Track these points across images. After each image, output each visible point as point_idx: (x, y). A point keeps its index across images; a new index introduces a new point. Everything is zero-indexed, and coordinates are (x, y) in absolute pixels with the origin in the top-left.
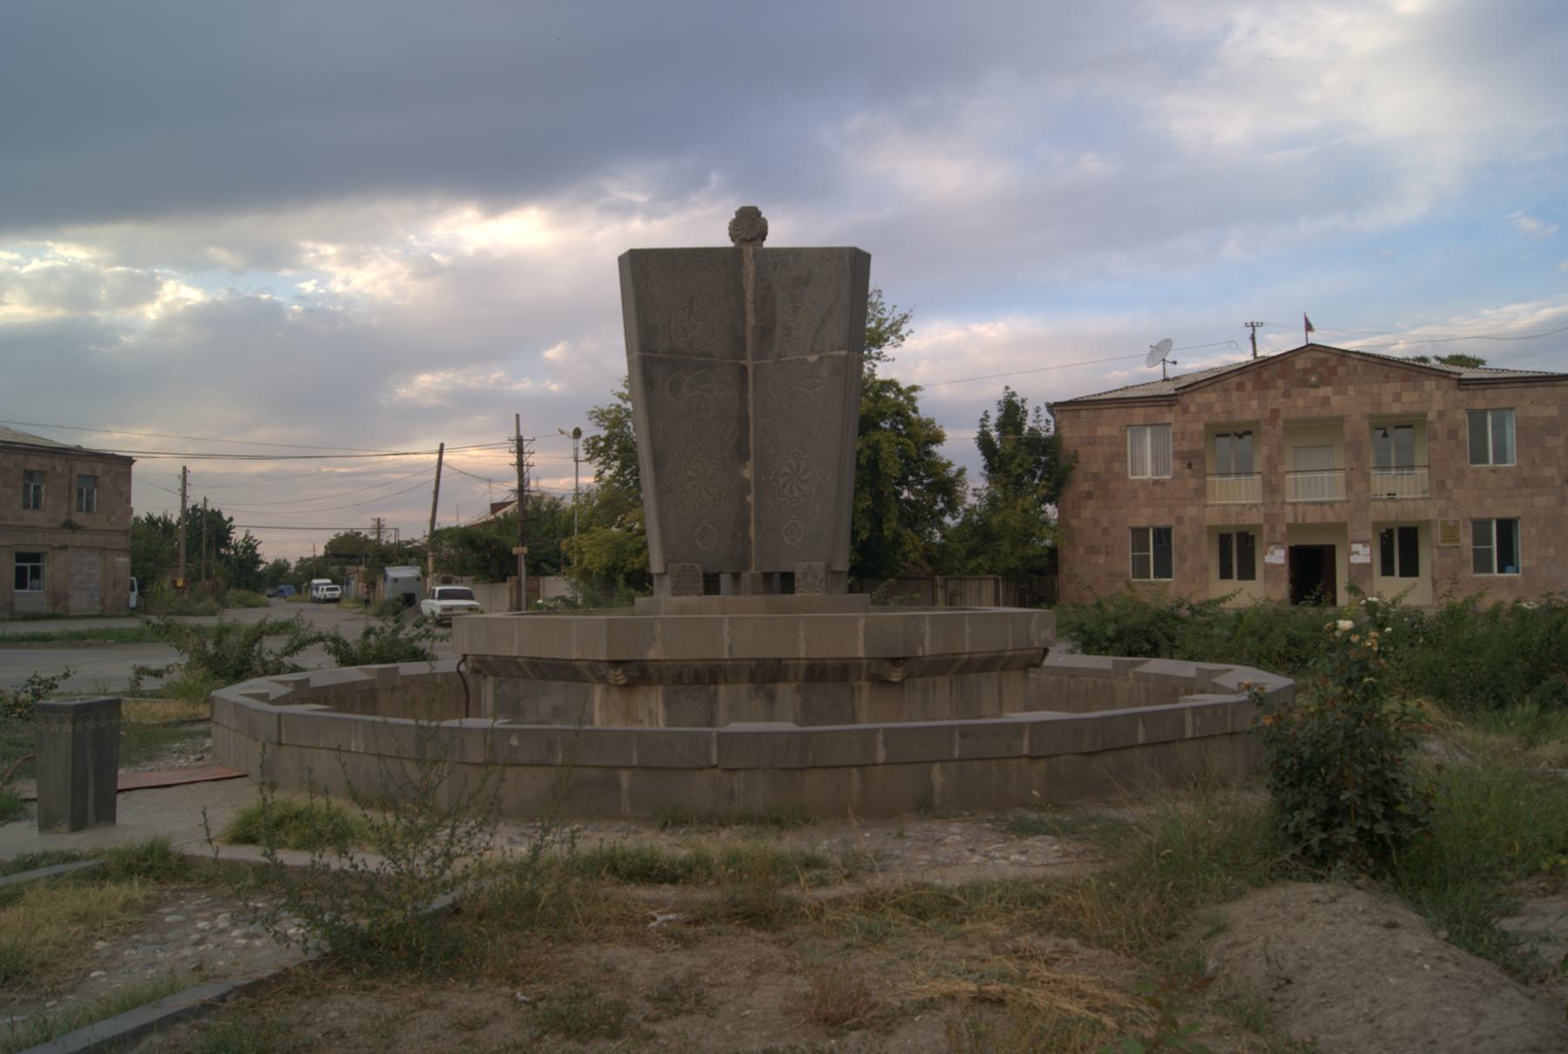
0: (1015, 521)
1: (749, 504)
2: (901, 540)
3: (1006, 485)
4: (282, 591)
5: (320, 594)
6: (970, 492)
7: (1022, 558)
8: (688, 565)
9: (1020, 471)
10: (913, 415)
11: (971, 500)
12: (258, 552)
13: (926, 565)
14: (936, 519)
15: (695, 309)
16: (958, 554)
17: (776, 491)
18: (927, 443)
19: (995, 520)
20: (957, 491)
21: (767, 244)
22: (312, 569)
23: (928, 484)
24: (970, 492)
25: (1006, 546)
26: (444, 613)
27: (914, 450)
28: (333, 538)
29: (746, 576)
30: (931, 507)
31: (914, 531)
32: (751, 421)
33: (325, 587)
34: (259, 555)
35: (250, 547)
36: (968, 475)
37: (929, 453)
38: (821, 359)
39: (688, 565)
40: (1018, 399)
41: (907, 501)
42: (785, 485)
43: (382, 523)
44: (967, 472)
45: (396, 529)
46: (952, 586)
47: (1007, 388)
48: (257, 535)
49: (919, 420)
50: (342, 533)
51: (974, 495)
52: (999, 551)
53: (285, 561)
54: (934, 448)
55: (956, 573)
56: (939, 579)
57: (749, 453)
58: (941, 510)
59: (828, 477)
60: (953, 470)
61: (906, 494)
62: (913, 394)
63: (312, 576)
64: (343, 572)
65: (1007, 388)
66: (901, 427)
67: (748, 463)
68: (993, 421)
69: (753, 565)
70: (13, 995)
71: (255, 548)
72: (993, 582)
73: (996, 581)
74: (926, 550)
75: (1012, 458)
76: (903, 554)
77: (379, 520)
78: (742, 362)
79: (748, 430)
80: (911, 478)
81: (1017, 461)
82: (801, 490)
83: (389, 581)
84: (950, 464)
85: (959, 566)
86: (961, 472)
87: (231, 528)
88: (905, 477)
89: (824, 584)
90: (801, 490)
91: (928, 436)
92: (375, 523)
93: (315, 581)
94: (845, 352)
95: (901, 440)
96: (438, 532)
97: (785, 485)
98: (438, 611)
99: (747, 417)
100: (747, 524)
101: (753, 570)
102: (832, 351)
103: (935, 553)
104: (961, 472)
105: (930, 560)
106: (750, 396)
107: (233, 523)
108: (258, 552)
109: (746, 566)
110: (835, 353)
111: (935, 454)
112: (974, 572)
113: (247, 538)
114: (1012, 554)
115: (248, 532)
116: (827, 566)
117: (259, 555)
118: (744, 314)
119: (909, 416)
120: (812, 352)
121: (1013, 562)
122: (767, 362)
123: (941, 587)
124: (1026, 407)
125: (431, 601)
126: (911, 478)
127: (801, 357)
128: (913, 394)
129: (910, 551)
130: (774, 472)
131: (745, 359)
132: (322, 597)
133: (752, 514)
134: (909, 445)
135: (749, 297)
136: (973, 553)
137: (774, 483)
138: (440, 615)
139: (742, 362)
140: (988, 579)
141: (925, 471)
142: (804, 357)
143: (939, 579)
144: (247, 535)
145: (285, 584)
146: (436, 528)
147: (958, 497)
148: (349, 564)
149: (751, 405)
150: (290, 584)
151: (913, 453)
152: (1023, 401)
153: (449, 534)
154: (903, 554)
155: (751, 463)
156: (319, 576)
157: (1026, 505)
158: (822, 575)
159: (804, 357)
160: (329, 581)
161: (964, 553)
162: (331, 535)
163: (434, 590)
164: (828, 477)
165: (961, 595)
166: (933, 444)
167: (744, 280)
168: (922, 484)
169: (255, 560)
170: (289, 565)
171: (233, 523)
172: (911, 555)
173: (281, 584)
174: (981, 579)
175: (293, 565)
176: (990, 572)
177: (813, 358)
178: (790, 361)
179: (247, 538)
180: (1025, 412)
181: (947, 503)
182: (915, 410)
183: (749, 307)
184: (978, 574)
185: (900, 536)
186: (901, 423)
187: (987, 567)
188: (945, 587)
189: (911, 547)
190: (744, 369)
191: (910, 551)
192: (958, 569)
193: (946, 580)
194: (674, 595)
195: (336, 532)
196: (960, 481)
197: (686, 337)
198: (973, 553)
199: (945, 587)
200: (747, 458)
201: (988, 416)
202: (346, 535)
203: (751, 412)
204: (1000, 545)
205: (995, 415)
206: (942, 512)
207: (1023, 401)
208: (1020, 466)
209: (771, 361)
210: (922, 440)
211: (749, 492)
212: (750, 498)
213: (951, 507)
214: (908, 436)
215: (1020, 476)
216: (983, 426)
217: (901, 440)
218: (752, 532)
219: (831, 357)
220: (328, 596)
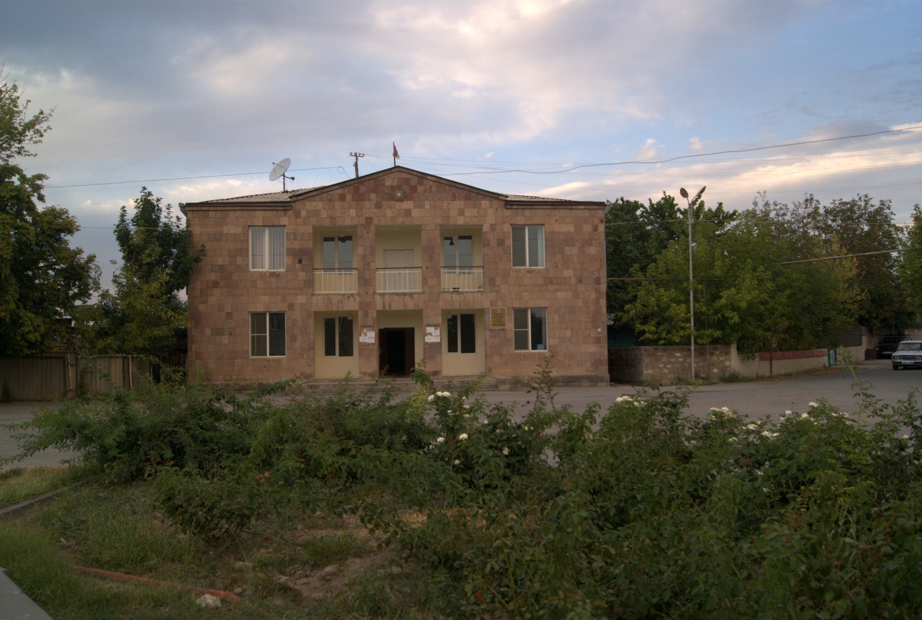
40: (153, 198)
60: (84, 256)
62: (39, 182)
65: (144, 188)
72: (121, 360)
76: (23, 335)
84: (80, 251)
86: (91, 259)
112: (104, 351)
123: (72, 365)
128: (39, 182)
129: (29, 332)
140: (117, 357)
143: (70, 358)
154: (23, 335)
174: (111, 357)
188: (76, 365)
189: (30, 328)
199: (76, 365)
205: (132, 212)
207: (158, 200)
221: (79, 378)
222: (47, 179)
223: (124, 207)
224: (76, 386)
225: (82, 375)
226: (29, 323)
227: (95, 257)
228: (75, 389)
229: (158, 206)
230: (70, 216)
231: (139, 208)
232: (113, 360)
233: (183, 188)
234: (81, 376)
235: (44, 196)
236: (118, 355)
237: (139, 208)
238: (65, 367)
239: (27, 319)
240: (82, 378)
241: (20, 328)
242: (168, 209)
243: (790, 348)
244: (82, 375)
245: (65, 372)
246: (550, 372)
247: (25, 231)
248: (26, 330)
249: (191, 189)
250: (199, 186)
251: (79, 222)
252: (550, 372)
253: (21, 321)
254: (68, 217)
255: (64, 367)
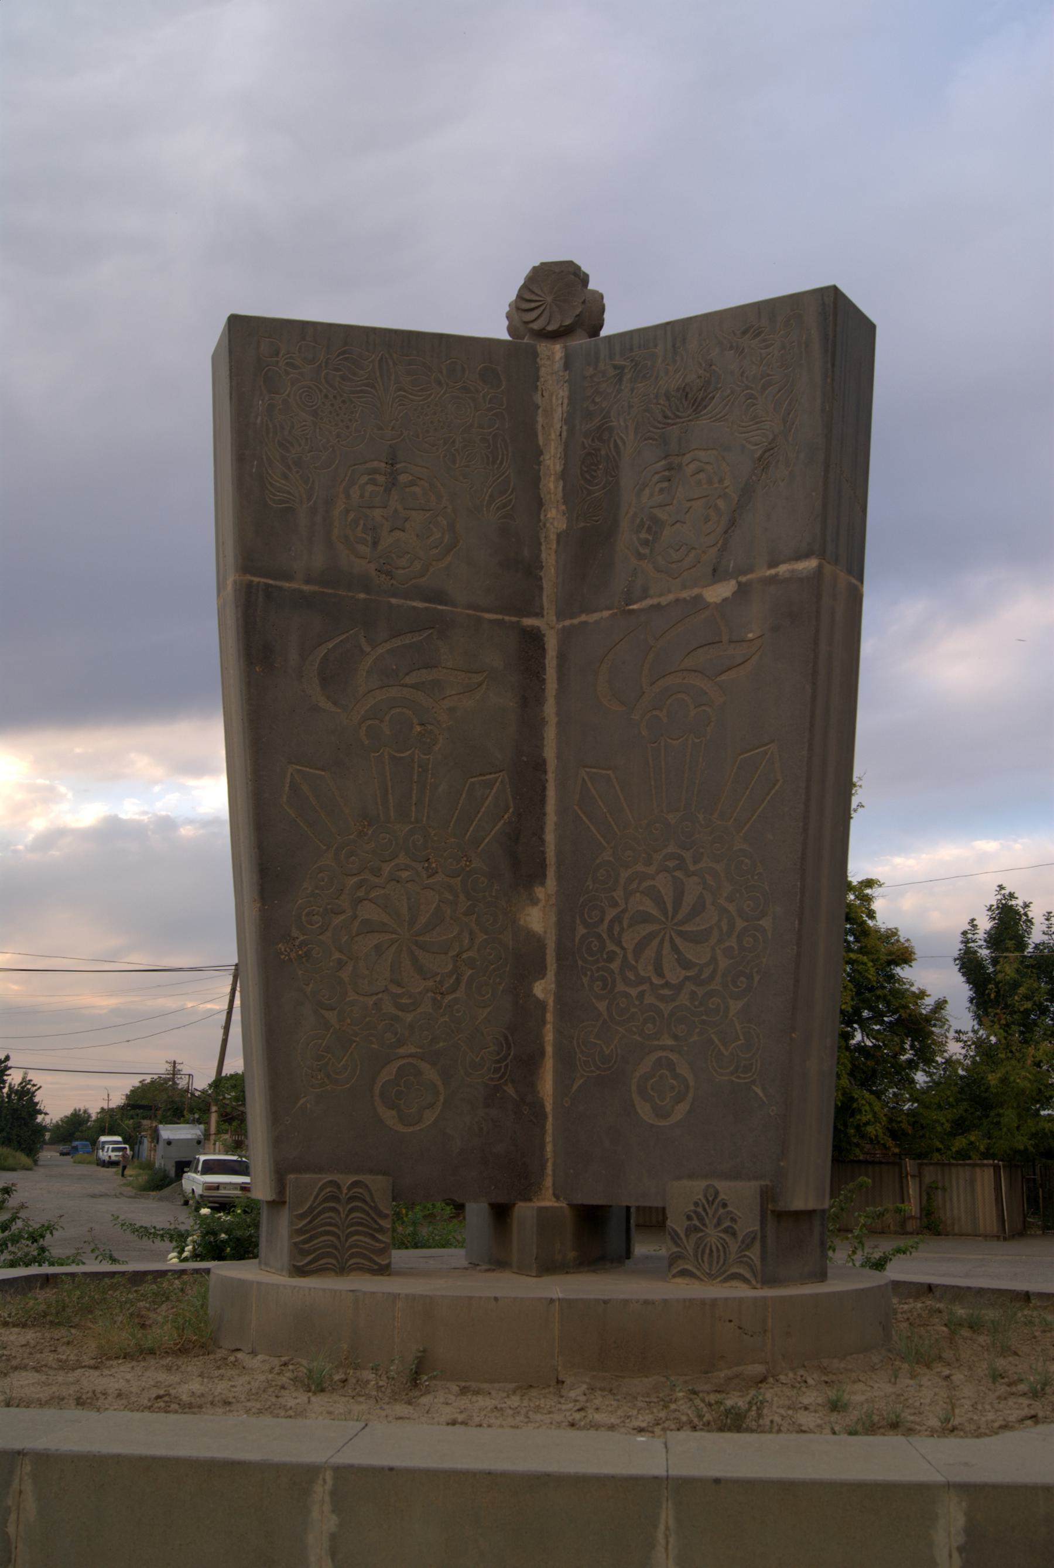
0: (1023, 1079)
1: (542, 1006)
2: (855, 1105)
3: (1007, 1025)
4: (76, 1148)
5: (103, 1155)
6: (951, 1034)
7: (1034, 1136)
8: (346, 1180)
9: (1028, 1005)
10: (870, 923)
11: (955, 1049)
12: (36, 1100)
13: (890, 1143)
14: (902, 1075)
15: (403, 478)
16: (939, 1129)
17: (614, 966)
18: (889, 963)
19: (993, 1079)
20: (932, 1033)
21: (604, 333)
22: (110, 1121)
23: (890, 1022)
24: (951, 1034)
25: (1009, 1116)
26: (207, 1193)
27: (872, 970)
28: (138, 1084)
29: (524, 1211)
30: (895, 1056)
31: (872, 1092)
32: (551, 776)
33: (111, 1146)
34: (37, 1103)
35: (25, 1094)
36: (949, 1011)
37: (891, 978)
38: (743, 590)
39: (346, 1180)
40: (1018, 903)
41: (861, 1048)
42: (639, 948)
43: (178, 1067)
44: (948, 1006)
45: (189, 1075)
46: (930, 1175)
47: (1001, 887)
48: (35, 1077)
49: (877, 931)
50: (148, 1079)
51: (958, 1040)
52: (998, 1123)
53: (85, 1111)
54: (898, 971)
55: (936, 1156)
56: (910, 1165)
57: (543, 865)
58: (910, 1061)
59: (766, 923)
60: (929, 1002)
61: (858, 1036)
62: (868, 891)
63: (103, 1132)
64: (138, 1127)
65: (1001, 887)
66: (851, 939)
67: (540, 892)
68: (981, 935)
69: (549, 1182)
70: (976, 948)
71: (33, 1094)
72: (992, 1170)
73: (996, 1168)
74: (891, 1120)
75: (1016, 985)
76: (858, 1128)
77: (175, 1063)
78: (528, 622)
79: (543, 801)
80: (866, 1014)
81: (1022, 990)
82: (684, 963)
83: (162, 1144)
84: (922, 994)
85: (941, 1146)
86: (940, 1005)
87: (8, 1068)
88: (857, 1011)
89: (754, 1254)
90: (684, 963)
91: (890, 953)
92: (169, 1067)
93: (103, 1139)
94: (812, 563)
95: (852, 955)
96: (227, 1078)
97: (639, 948)
98: (199, 1191)
99: (540, 766)
100: (531, 1062)
101: (547, 1201)
102: (772, 564)
103: (904, 1125)
104: (940, 1005)
105: (895, 1134)
106: (550, 709)
107: (10, 1063)
108: (36, 1100)
109: (528, 1189)
110: (783, 569)
111: (900, 981)
112: (963, 1155)
113: (25, 1082)
114: (1018, 1128)
115: (26, 1073)
116: (767, 1196)
117: (37, 1103)
118: (539, 504)
119: (864, 922)
120: (717, 574)
121: (1021, 1142)
122: (595, 617)
123: (913, 1176)
124: (1030, 914)
125: (194, 1175)
126: (866, 1014)
127: (685, 594)
128: (868, 891)
129: (867, 1123)
130: (611, 913)
131: (540, 614)
132: (107, 1159)
133: (549, 1036)
134: (865, 964)
135: (552, 461)
136: (960, 1126)
137: (611, 946)
138: (201, 1196)
139: (528, 622)
140: (984, 1165)
141: (888, 1004)
142: (696, 591)
143: (910, 1165)
144: (24, 1078)
145: (82, 1140)
146: (223, 1074)
147: (934, 1042)
148: (144, 1118)
149: (550, 734)
150: (86, 1140)
151: (872, 974)
152: (1026, 905)
153: (233, 1082)
154: (858, 1128)
155: (548, 889)
156: (111, 1133)
157: (1040, 1055)
158: (748, 1223)
159: (696, 591)
160: (119, 1139)
161: (947, 1126)
162: (135, 1082)
163: (198, 1160)
164: (766, 923)
165: (944, 1189)
166: (897, 965)
167: (540, 419)
168: (882, 1023)
169: (33, 1109)
170: (89, 1116)
171: (10, 1063)
172: (870, 1129)
173: (77, 1140)
174: (974, 1165)
175: (94, 1117)
176: (986, 1155)
177: (719, 592)
178: (658, 607)
179: (25, 1082)
180: (1030, 921)
181: (918, 1052)
182: (871, 915)
183: (552, 486)
184: (970, 1158)
185: (852, 1100)
186: (851, 932)
187: (982, 1148)
188: (920, 1175)
189: (870, 1116)
190: (534, 639)
191: (867, 1123)
192: (938, 1150)
193: (920, 1165)
194: (300, 1272)
195: (141, 1078)
196: (937, 1020)
197: (375, 544)
198: (960, 1126)
199: (920, 1175)
200: (538, 875)
201: (975, 926)
202: (153, 1082)
203: (550, 753)
204: (999, 1115)
205: (985, 924)
206: (912, 1065)
207: (1026, 905)
208: (1027, 998)
209: (606, 614)
210: (884, 958)
211: (541, 972)
212: (543, 989)
213: (925, 1056)
214: (862, 951)
215: (1027, 1013)
216: (966, 942)
217: (852, 955)
218: (547, 1086)
219: (773, 580)
220: (113, 1158)
221: (925, 1198)
222: (880, 886)
223: (973, 920)
224: (921, 1210)
225: (929, 1193)
226: (867, 1108)
227: (945, 1002)
228: (918, 1215)
229: (1026, 914)
230: (902, 940)
231: (994, 919)
232: (978, 1170)
233: (898, 860)
234: (928, 1194)
235: (874, 912)
236: (985, 1162)
237: (994, 919)
238: (902, 1178)
239: (864, 1102)
240: (929, 1198)
241: (852, 1115)
242: (1047, 920)
243: (246, 1132)
244: (929, 1193)
245: (902, 1188)
246: (57, 1230)
247: (860, 967)
248: (864, 1119)
249: (911, 862)
250: (924, 856)
251: (919, 950)
252: (57, 1230)
253: (855, 1105)
254: (898, 941)
255: (901, 1177)
